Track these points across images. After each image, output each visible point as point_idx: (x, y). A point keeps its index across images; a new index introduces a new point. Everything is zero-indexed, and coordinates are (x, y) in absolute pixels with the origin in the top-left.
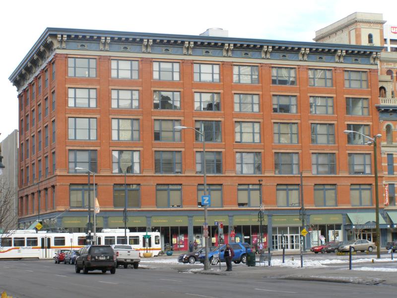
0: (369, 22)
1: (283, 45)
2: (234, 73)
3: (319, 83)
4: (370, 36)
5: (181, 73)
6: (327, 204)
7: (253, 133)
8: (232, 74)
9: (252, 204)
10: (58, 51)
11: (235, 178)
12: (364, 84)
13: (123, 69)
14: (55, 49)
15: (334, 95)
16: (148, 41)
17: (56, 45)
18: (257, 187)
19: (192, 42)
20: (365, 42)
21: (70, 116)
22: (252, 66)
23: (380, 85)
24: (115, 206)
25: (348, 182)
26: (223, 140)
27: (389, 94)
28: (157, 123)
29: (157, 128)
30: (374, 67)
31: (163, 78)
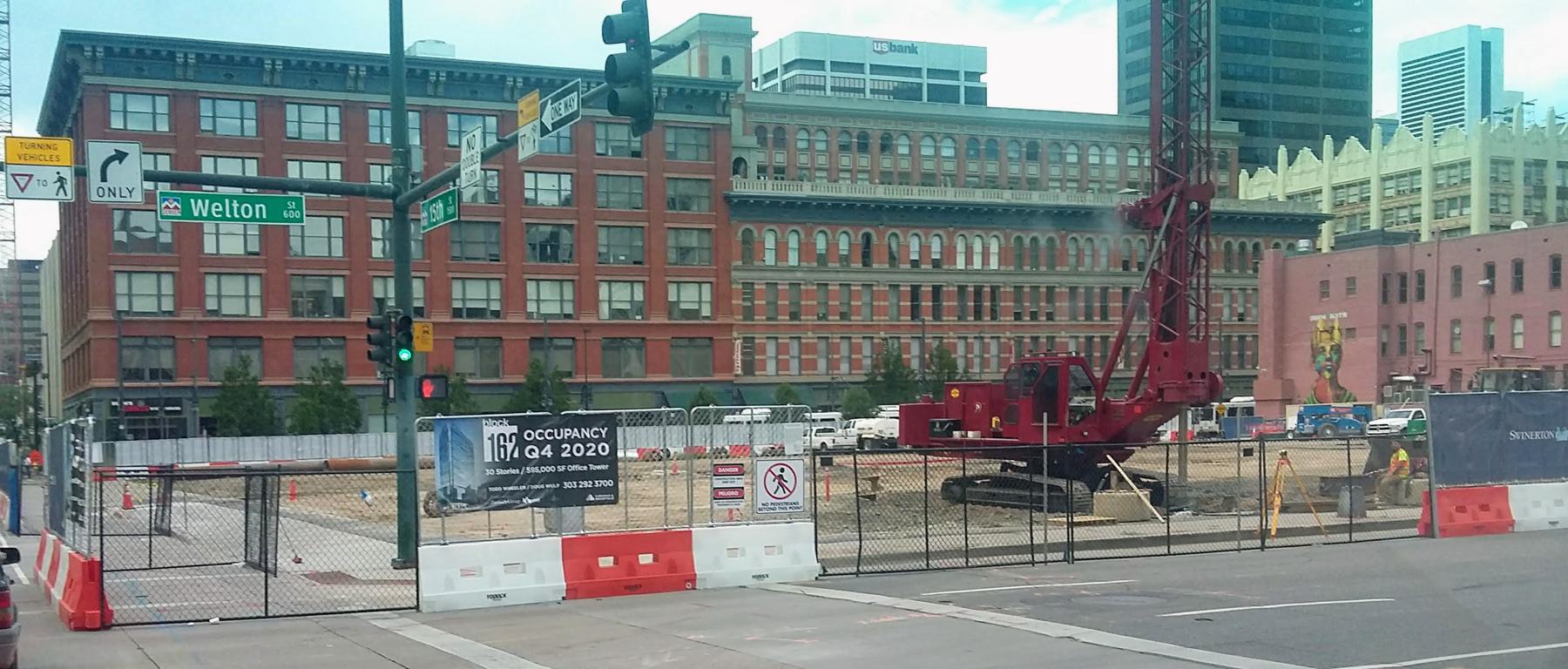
0: (726, 35)
2: (337, 128)
4: (726, 62)
5: (344, 125)
7: (247, 297)
8: (366, 127)
12: (704, 152)
15: (644, 174)
16: (357, 69)
17: (84, 67)
20: (715, 73)
23: (735, 155)
27: (753, 171)
28: (670, 185)
29: (670, 193)
30: (725, 121)
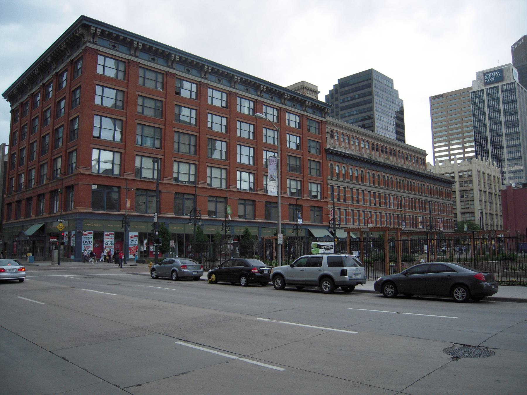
1: (122, 35)
3: (150, 84)
6: (149, 211)
9: (247, 216)
10: (89, 45)
11: (237, 193)
13: (217, 99)
14: (86, 42)
18: (192, 197)
19: (99, 29)
21: (97, 113)
22: (118, 60)
24: (93, 208)
25: (309, 204)
26: (228, 159)
31: (106, 74)
